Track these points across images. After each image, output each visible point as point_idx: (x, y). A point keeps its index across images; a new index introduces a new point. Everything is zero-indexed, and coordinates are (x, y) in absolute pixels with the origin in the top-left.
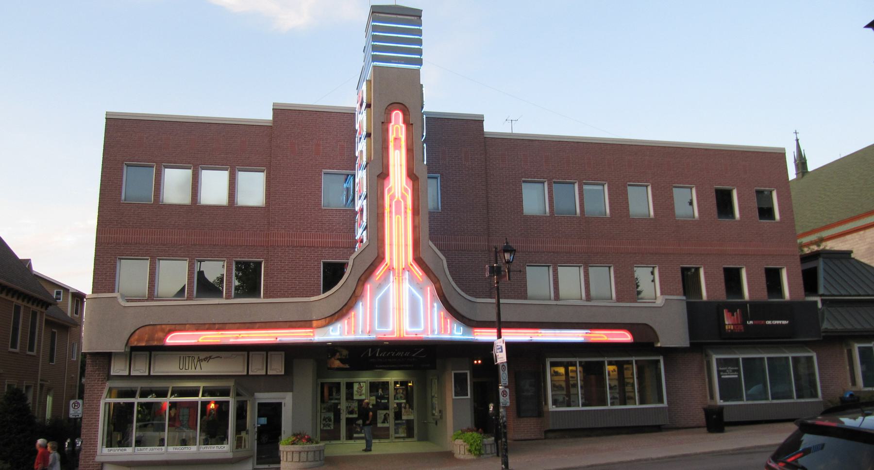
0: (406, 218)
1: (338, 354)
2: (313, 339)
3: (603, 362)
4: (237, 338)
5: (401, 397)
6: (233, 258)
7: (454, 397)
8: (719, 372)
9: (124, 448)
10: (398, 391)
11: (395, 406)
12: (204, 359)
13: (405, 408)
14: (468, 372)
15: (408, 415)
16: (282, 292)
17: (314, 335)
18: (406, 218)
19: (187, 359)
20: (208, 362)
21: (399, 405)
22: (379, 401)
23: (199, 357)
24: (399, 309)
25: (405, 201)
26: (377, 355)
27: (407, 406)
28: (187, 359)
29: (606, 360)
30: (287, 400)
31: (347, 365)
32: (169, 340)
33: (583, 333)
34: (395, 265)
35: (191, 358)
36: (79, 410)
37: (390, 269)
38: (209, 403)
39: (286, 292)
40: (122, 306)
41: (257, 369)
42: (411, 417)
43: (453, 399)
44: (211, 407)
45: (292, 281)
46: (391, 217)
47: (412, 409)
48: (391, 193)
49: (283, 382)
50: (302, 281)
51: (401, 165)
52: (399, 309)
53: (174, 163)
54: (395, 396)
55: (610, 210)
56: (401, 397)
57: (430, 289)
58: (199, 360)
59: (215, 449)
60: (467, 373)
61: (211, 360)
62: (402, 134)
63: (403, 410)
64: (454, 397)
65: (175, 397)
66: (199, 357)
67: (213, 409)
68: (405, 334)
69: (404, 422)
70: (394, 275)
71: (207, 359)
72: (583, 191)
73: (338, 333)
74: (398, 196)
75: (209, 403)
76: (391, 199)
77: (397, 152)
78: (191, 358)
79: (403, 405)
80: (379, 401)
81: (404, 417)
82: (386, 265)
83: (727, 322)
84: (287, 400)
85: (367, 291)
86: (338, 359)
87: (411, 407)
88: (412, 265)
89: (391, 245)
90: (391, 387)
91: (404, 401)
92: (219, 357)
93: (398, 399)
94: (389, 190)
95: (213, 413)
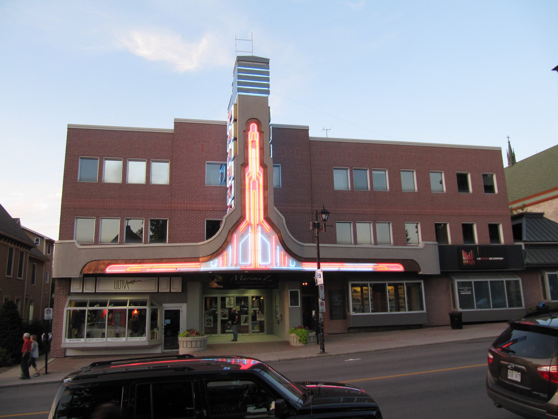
0: (259, 192)
1: (216, 279)
2: (200, 269)
3: (385, 284)
4: (152, 268)
5: (256, 306)
6: (149, 217)
7: (290, 306)
8: (459, 290)
9: (79, 339)
10: (254, 302)
11: (252, 312)
12: (131, 282)
13: (259, 313)
14: (299, 290)
15: (260, 318)
16: (180, 239)
17: (200, 267)
18: (259, 192)
19: (120, 282)
20: (133, 284)
21: (255, 311)
22: (242, 309)
23: (127, 281)
24: (255, 250)
25: (259, 181)
26: (241, 279)
27: (260, 312)
28: (120, 282)
29: (387, 282)
30: (183, 308)
31: (222, 286)
32: (108, 270)
33: (372, 266)
34: (252, 222)
35: (122, 282)
36: (324, 308)
37: (249, 224)
38: (133, 310)
39: (182, 239)
40: (78, 248)
41: (164, 288)
42: (263, 319)
43: (289, 308)
44: (135, 313)
45: (186, 232)
46: (250, 191)
47: (263, 314)
48: (250, 176)
49: (181, 297)
50: (193, 232)
51: (256, 158)
52: (255, 250)
53: (111, 157)
54: (252, 306)
55: (390, 187)
56: (256, 306)
57: (274, 237)
58: (127, 283)
59: (137, 339)
60: (298, 291)
61: (134, 283)
62: (256, 138)
63: (257, 315)
64: (290, 306)
65: (112, 306)
66: (127, 281)
67: (136, 314)
68: (258, 266)
69: (258, 322)
70: (251, 229)
71: (132, 282)
72: (372, 175)
73: (216, 265)
74: (254, 178)
75: (133, 310)
76: (250, 180)
77: (254, 149)
78: (122, 282)
79: (257, 311)
80: (242, 309)
81: (258, 319)
82: (247, 222)
83: (464, 259)
84: (183, 308)
85: (234, 239)
86: (216, 282)
87: (263, 312)
88: (263, 222)
89: (250, 209)
90: (250, 300)
91: (258, 309)
92: (139, 281)
93: (254, 308)
94: (249, 174)
95: (136, 316)
